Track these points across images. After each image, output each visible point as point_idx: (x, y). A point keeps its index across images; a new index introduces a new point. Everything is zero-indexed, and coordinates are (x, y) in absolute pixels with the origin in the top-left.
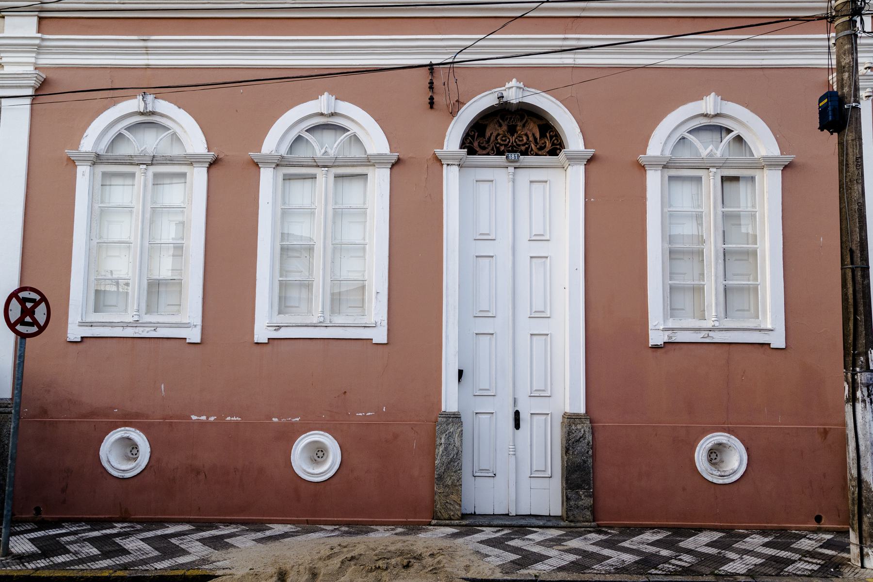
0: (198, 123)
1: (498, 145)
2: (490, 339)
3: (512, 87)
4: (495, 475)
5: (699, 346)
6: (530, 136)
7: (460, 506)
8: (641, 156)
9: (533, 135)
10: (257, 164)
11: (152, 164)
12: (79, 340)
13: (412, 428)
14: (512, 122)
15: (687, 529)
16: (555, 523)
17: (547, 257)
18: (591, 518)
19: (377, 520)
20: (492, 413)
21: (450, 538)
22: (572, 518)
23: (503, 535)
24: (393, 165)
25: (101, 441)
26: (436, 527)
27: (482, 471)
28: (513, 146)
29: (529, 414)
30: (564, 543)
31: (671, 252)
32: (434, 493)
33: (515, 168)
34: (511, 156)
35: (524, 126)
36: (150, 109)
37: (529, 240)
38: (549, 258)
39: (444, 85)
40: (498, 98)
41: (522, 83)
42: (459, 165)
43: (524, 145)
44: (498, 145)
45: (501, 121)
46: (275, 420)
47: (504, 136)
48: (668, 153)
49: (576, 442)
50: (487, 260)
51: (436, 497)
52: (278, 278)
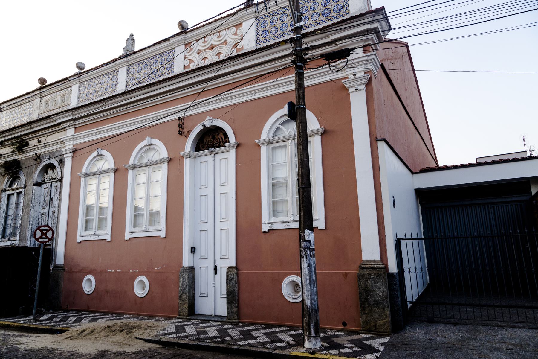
0: (312, 113)
5: (284, 231)
9: (222, 138)
10: (259, 145)
11: (100, 174)
12: (79, 242)
18: (236, 317)
22: (229, 317)
25: (281, 283)
28: (214, 144)
31: (273, 186)
36: (99, 154)
43: (218, 143)
46: (131, 271)
50: (204, 197)
52: (133, 213)
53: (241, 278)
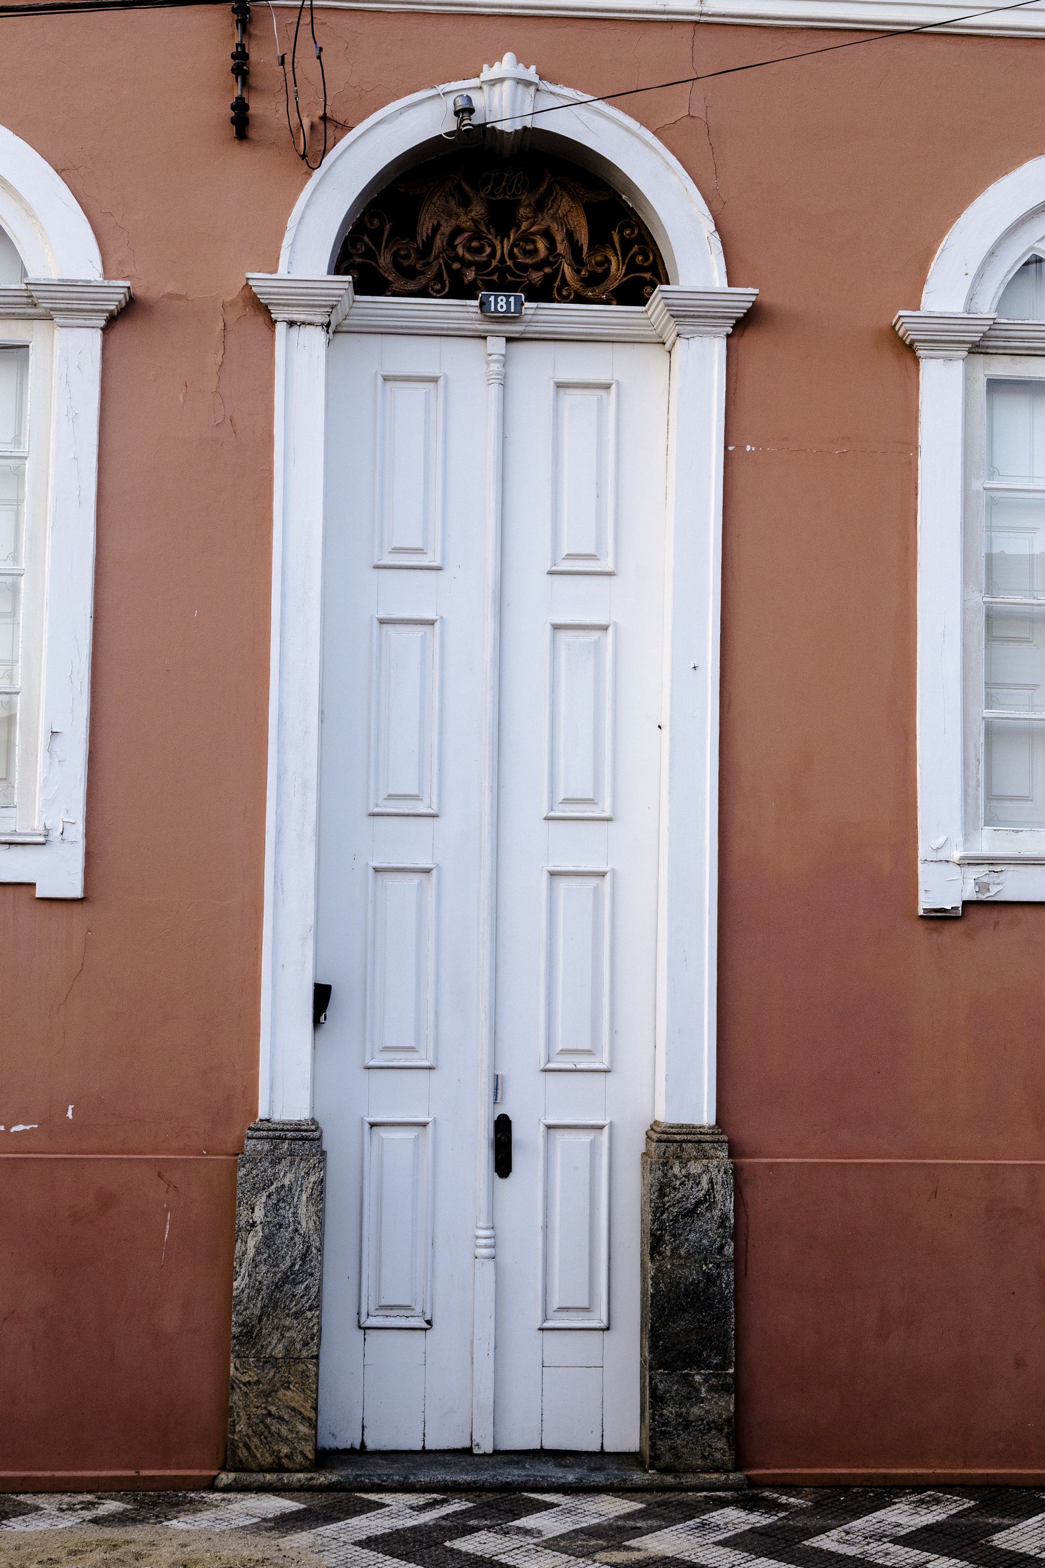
1: (456, 266)
2: (420, 886)
3: (501, 80)
4: (429, 1322)
6: (559, 237)
7: (314, 1425)
8: (901, 313)
9: (570, 235)
10: (911, 348)
13: (160, 1175)
14: (504, 193)
15: (1028, 1488)
16: (616, 1477)
17: (605, 628)
18: (728, 1458)
19: (39, 1474)
20: (424, 1125)
21: (270, 1529)
22: (667, 1459)
23: (443, 1518)
24: (113, 321)
26: (231, 1496)
27: (388, 1312)
28: (502, 269)
29: (542, 1128)
30: (633, 1543)
32: (231, 1385)
33: (509, 340)
34: (496, 303)
35: (540, 207)
37: (551, 573)
38: (610, 629)
39: (283, 63)
40: (457, 113)
41: (533, 68)
42: (328, 325)
43: (538, 267)
44: (456, 266)
45: (466, 188)
47: (477, 235)
48: (986, 307)
49: (684, 1216)
51: (236, 1397)
53: (757, 1195)
